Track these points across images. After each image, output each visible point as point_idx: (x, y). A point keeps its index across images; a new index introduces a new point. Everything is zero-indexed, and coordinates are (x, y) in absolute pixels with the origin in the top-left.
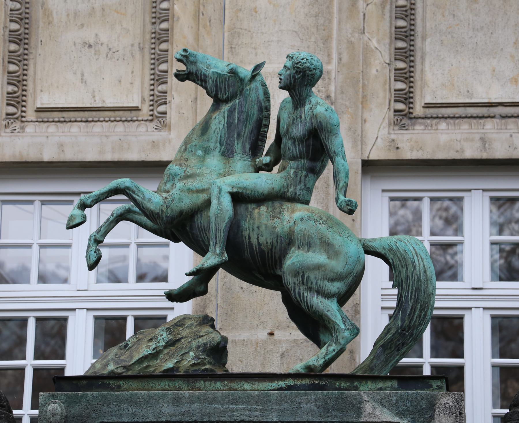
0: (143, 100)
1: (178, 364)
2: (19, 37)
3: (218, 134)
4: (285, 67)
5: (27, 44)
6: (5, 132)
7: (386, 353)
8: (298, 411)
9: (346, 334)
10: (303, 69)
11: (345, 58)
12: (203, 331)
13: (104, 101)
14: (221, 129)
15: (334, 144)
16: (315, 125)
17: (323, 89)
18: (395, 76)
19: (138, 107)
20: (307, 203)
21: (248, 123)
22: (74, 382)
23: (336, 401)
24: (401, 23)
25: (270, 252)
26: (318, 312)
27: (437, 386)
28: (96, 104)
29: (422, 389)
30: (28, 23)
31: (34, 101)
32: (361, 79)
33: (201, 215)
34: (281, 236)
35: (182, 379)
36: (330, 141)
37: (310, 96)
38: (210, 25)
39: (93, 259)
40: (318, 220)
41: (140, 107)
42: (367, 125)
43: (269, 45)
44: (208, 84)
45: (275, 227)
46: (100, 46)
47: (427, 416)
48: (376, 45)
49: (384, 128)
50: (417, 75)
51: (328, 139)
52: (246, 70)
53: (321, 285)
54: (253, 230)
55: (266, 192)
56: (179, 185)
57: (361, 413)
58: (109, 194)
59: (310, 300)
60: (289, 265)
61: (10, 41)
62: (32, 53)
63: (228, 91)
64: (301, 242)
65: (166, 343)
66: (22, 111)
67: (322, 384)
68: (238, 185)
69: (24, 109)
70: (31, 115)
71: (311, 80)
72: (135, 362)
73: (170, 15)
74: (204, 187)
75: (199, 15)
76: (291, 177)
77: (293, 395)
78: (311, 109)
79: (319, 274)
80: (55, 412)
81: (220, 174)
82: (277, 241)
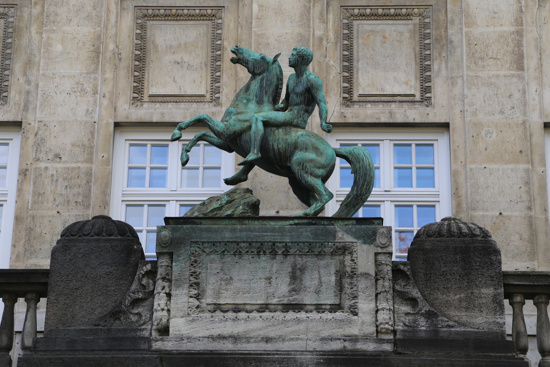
0: (207, 91)
4: (292, 54)
9: (327, 197)
15: (321, 95)
16: (309, 85)
20: (304, 128)
24: (346, 53)
39: (185, 160)
45: (287, 140)
48: (333, 64)
50: (355, 80)
52: (270, 58)
55: (282, 121)
56: (234, 117)
57: (336, 237)
61: (135, 60)
67: (314, 222)
70: (146, 98)
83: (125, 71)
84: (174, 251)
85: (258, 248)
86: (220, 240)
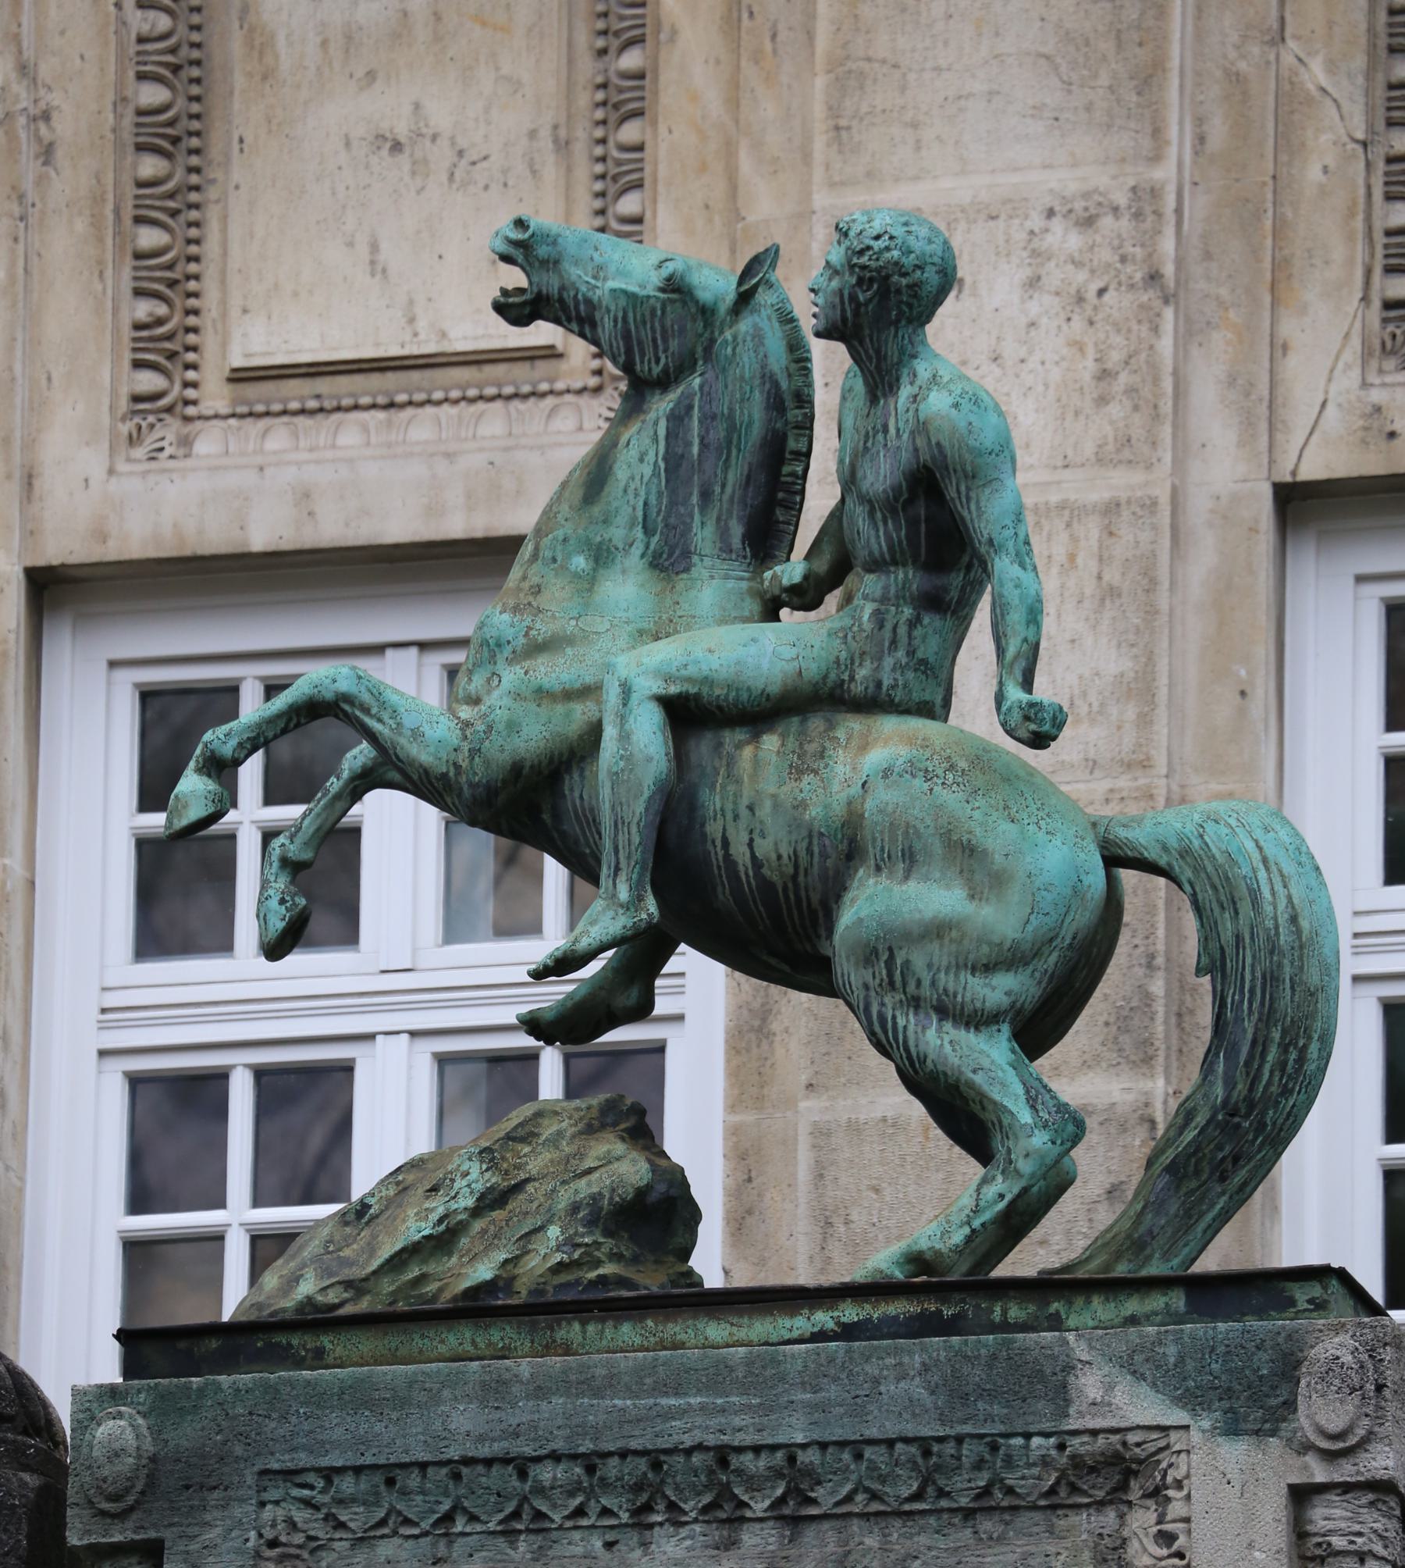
1: (509, 1267)
2: (169, 131)
3: (636, 495)
5: (197, 152)
6: (129, 460)
7: (1184, 1190)
8: (870, 1407)
9: (1040, 1140)
10: (879, 270)
11: (1218, 131)
12: (593, 1153)
13: (444, 335)
14: (645, 479)
15: (988, 515)
16: (925, 456)
17: (1138, 250)
18: (1386, 184)
19: (552, 347)
21: (734, 452)
22: (182, 1345)
23: (990, 1367)
25: (790, 885)
26: (945, 1074)
27: (1309, 1301)
28: (419, 343)
29: (1261, 1313)
30: (198, 81)
31: (224, 345)
32: (1269, 205)
33: (582, 770)
34: (821, 834)
35: (514, 1319)
36: (973, 507)
37: (914, 356)
38: (775, 52)
40: (940, 772)
41: (560, 348)
42: (1292, 364)
43: (960, 110)
44: (600, 330)
45: (802, 805)
46: (428, 143)
47: (1273, 1402)
48: (1323, 80)
49: (1348, 366)
51: (968, 499)
52: (716, 282)
53: (951, 987)
54: (736, 817)
55: (774, 689)
57: (1068, 1402)
58: (290, 720)
59: (917, 1039)
60: (847, 927)
61: (140, 148)
62: (213, 181)
63: (665, 351)
64: (882, 850)
65: (478, 1200)
66: (187, 384)
67: (948, 1312)
68: (683, 672)
69: (191, 375)
70: (215, 395)
71: (910, 306)
72: (382, 1266)
73: (648, 21)
74: (589, 679)
75: (739, 20)
76: (862, 630)
77: (856, 1356)
78: (915, 401)
79: (940, 953)
80: (117, 1446)
81: (641, 632)
82: (809, 851)
83: (81, 225)
84: (167, 1534)
85: (638, 1488)
86: (424, 1456)
